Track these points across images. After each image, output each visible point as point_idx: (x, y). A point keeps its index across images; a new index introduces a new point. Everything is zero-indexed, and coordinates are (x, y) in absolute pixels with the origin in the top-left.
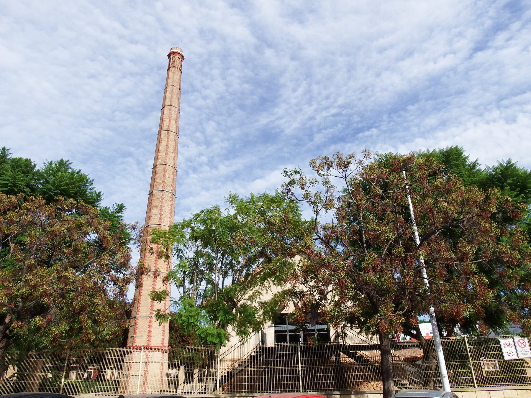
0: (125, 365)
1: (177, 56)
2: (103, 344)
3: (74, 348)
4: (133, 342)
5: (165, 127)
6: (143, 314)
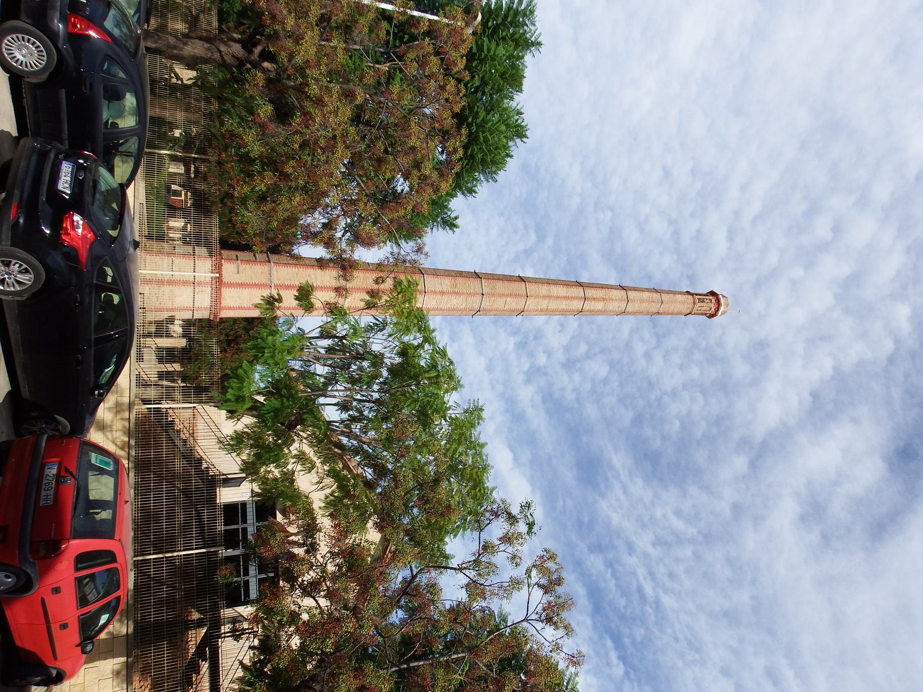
1: (713, 307)
2: (227, 211)
3: (221, 168)
4: (229, 259)
5: (590, 293)
6: (274, 273)
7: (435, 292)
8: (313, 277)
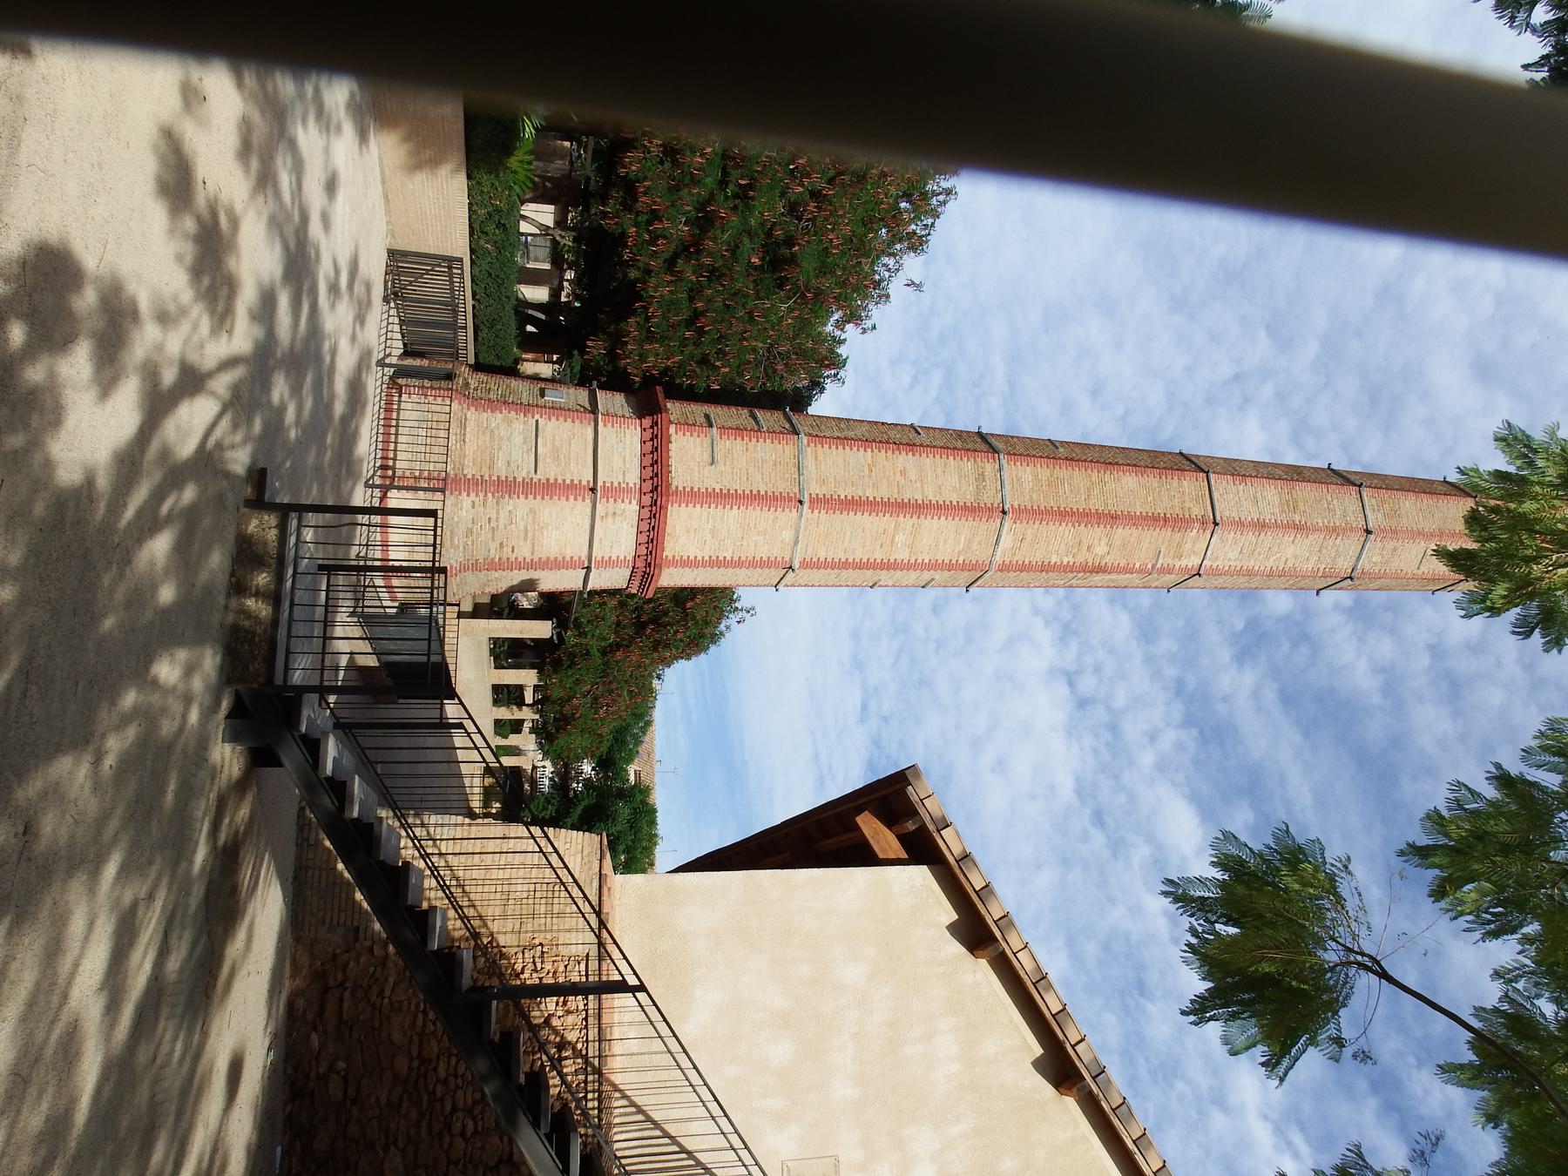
0: (582, 395)
3: (675, 163)
4: (687, 424)
6: (809, 463)
7: (1240, 524)
8: (912, 475)
